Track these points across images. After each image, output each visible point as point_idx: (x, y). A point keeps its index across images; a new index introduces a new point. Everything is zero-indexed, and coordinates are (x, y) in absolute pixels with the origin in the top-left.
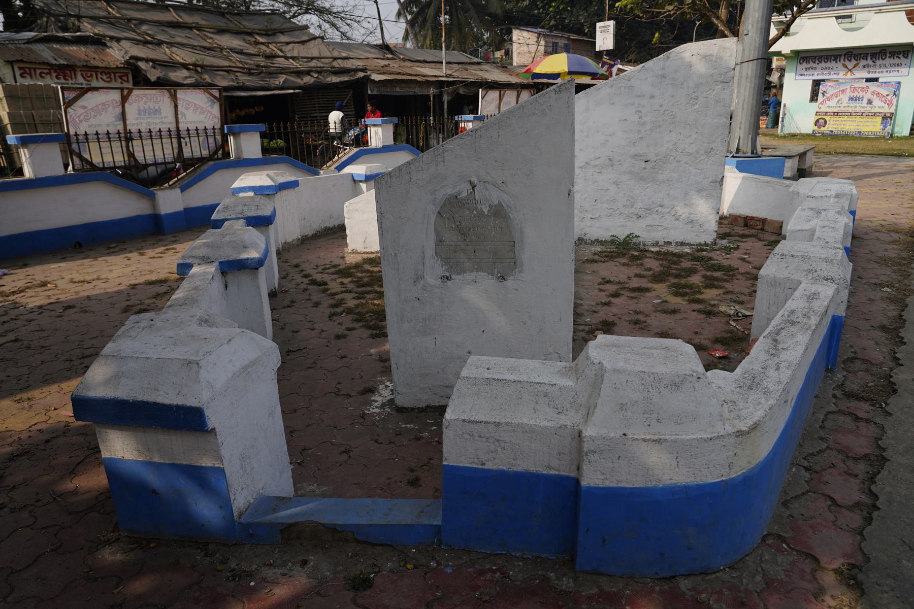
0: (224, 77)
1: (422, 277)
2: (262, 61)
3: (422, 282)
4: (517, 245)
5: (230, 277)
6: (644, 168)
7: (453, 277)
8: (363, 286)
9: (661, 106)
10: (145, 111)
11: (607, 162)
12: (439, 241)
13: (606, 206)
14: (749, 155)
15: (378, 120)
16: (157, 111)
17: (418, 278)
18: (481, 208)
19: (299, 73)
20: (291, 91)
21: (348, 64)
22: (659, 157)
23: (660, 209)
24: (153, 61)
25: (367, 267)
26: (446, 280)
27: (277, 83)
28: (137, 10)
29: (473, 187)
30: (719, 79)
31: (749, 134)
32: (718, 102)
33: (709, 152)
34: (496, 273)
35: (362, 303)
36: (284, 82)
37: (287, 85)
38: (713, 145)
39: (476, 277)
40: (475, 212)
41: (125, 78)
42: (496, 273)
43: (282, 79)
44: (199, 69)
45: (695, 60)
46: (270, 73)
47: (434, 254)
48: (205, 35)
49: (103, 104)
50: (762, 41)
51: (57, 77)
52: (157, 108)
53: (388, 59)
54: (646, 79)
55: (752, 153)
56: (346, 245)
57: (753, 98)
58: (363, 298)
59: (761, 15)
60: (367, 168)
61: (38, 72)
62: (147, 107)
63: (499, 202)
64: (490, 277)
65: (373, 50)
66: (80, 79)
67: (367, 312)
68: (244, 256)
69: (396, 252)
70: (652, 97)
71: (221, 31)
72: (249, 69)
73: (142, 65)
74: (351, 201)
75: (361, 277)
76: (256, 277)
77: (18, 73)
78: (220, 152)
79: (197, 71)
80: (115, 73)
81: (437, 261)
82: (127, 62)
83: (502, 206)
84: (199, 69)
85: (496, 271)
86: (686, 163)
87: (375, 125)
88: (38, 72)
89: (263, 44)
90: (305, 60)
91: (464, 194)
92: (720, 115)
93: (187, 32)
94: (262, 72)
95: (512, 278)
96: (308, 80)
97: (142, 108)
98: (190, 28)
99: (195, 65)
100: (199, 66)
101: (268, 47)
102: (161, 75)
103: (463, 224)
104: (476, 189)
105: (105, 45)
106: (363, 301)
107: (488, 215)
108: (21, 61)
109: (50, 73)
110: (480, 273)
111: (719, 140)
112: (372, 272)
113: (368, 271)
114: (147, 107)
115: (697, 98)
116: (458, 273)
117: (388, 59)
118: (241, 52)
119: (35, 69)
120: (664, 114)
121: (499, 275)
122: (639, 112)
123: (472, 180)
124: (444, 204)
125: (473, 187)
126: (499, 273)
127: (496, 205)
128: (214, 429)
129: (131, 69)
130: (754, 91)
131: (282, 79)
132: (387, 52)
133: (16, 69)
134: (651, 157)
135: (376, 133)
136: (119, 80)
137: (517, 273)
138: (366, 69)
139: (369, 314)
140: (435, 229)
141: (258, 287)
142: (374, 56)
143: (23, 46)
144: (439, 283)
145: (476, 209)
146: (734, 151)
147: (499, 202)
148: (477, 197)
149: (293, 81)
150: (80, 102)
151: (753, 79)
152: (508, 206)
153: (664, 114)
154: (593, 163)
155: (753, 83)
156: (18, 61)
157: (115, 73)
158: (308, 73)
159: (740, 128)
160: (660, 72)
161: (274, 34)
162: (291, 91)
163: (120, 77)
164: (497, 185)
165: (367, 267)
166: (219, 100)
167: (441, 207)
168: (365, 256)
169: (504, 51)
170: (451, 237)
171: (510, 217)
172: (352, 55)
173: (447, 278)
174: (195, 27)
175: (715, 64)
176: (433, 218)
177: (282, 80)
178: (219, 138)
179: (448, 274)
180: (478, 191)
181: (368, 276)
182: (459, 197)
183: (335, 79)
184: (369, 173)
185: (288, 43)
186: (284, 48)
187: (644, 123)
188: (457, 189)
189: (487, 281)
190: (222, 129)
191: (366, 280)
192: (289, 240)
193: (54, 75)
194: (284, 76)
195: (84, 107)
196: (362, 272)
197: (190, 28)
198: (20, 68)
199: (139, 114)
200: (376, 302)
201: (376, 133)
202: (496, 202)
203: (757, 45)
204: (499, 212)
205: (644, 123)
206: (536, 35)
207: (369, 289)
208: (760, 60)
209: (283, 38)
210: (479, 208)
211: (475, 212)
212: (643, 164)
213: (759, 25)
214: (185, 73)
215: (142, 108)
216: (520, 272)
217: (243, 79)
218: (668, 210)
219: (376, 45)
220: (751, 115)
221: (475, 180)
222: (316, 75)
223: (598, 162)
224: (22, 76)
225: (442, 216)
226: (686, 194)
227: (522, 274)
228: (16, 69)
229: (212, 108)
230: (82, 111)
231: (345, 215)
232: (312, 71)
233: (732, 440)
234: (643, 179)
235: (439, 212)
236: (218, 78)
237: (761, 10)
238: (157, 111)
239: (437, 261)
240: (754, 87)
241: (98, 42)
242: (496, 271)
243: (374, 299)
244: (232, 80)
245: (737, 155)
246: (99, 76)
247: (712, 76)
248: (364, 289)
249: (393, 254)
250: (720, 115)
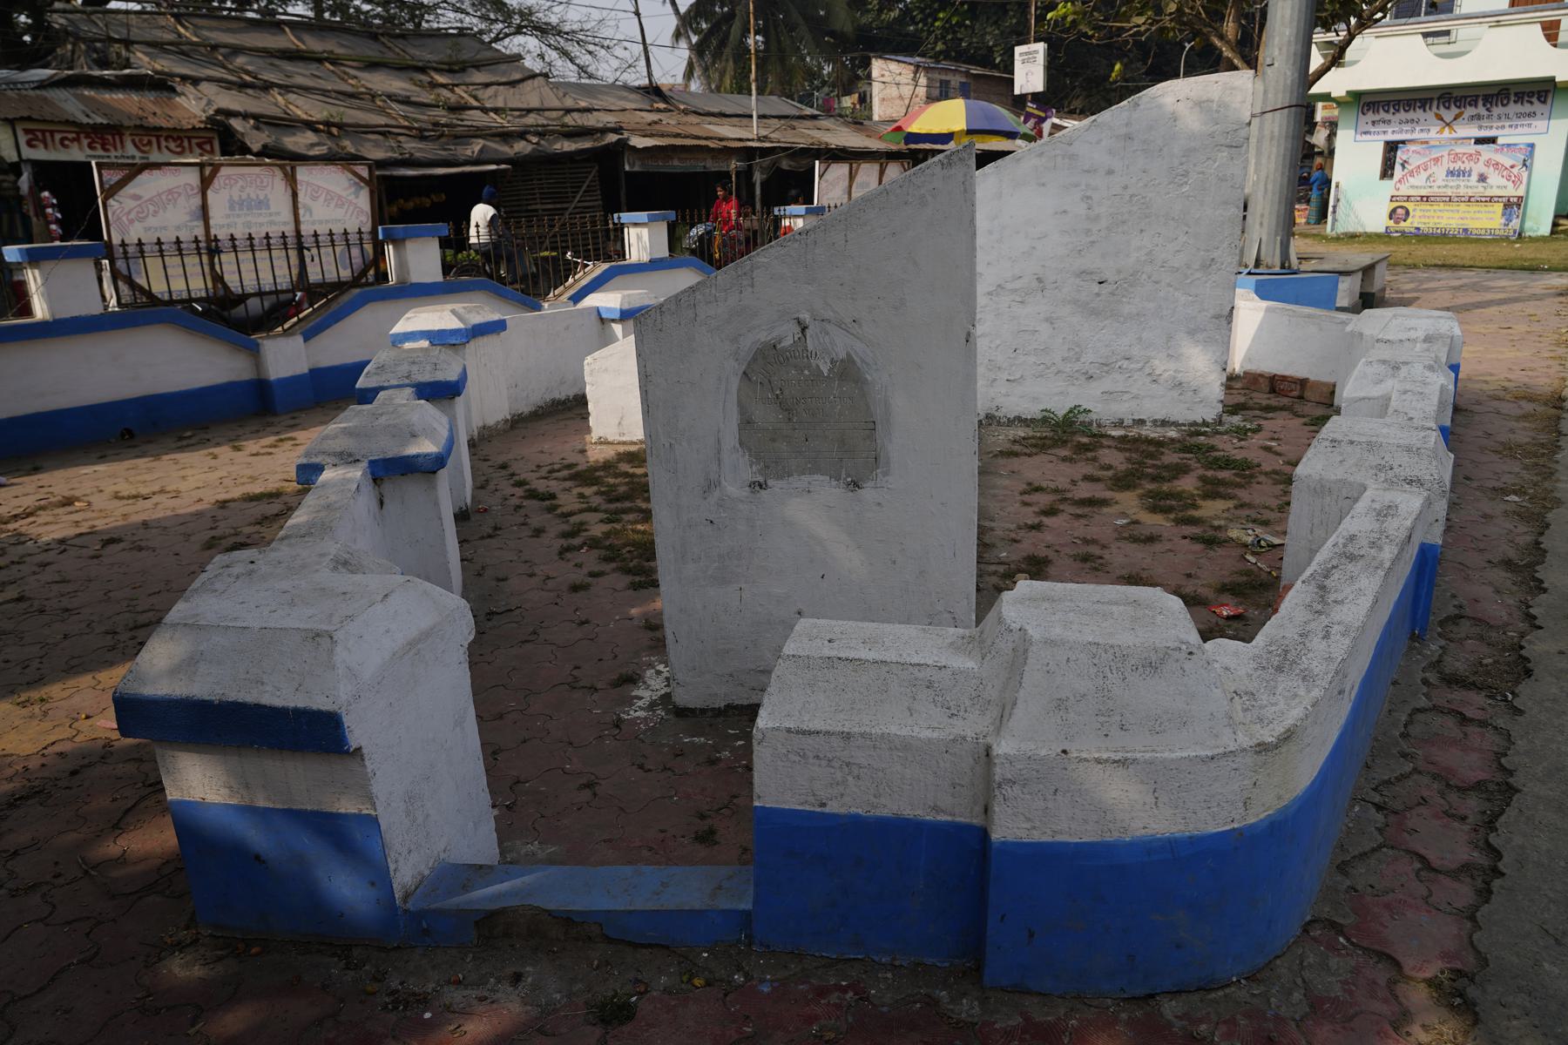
0: (377, 144)
1: (718, 484)
2: (443, 116)
3: (717, 493)
4: (879, 427)
5: (387, 487)
6: (1098, 295)
7: (770, 483)
8: (618, 500)
9: (1126, 187)
10: (241, 203)
11: (1035, 284)
12: (746, 422)
13: (1032, 359)
14: (1277, 269)
15: (642, 216)
16: (262, 204)
17: (711, 485)
18: (818, 366)
19: (506, 136)
20: (493, 167)
21: (591, 120)
22: (1122, 277)
23: (1125, 364)
24: (256, 117)
25: (625, 467)
26: (757, 488)
27: (469, 152)
28: (229, 30)
29: (804, 329)
30: (1223, 142)
31: (1276, 235)
32: (1222, 179)
33: (1208, 265)
34: (843, 476)
35: (615, 529)
36: (481, 151)
37: (485, 156)
38: (1215, 254)
39: (809, 483)
40: (806, 372)
41: (208, 147)
42: (843, 476)
43: (477, 146)
44: (335, 130)
45: (1182, 109)
46: (456, 137)
47: (738, 445)
48: (345, 73)
49: (170, 192)
50: (1296, 75)
51: (90, 146)
52: (262, 198)
53: (659, 110)
54: (1098, 142)
55: (1283, 267)
56: (588, 430)
57: (1283, 173)
58: (618, 521)
59: (1295, 31)
60: (624, 298)
61: (58, 137)
62: (244, 196)
63: (848, 355)
64: (834, 483)
65: (633, 96)
66: (131, 150)
67: (625, 545)
68: (412, 450)
69: (673, 442)
70: (1110, 172)
71: (372, 66)
72: (421, 130)
73: (236, 124)
74: (596, 354)
75: (614, 485)
76: (433, 487)
77: (22, 139)
78: (372, 272)
79: (331, 134)
80: (189, 139)
81: (743, 456)
82: (210, 119)
83: (854, 362)
84: (335, 130)
85: (844, 472)
86: (1169, 285)
87: (636, 225)
88: (58, 137)
89: (444, 86)
90: (517, 113)
91: (788, 342)
92: (1226, 203)
93: (313, 68)
94: (442, 135)
95: (870, 484)
96: (522, 147)
97: (236, 198)
98: (318, 60)
99: (328, 124)
100: (334, 125)
101: (452, 91)
102: (268, 140)
103: (786, 392)
104: (808, 333)
105: (173, 90)
106: (618, 526)
107: (828, 377)
108: (29, 119)
109: (77, 140)
110: (816, 477)
111: (1225, 245)
112: (633, 475)
113: (626, 475)
114: (244, 196)
115: (1186, 174)
116: (779, 477)
117: (659, 110)
118: (406, 101)
119: (52, 133)
120: (1130, 201)
121: (849, 479)
122: (1089, 198)
123: (801, 316)
124: (754, 359)
125: (804, 329)
126: (848, 476)
127: (842, 361)
128: (359, 749)
129: (220, 134)
130: (1284, 159)
131: (477, 146)
132: (657, 99)
133: (20, 134)
134: (1109, 275)
135: (639, 238)
136: (198, 151)
137: (880, 475)
138: (621, 128)
139: (628, 549)
140: (740, 404)
141: (436, 504)
142: (634, 106)
143: (31, 93)
144: (744, 494)
145: (809, 367)
146: (1252, 263)
147: (848, 355)
148: (810, 347)
149: (496, 150)
150: (130, 189)
151: (1282, 141)
152: (863, 361)
153: (1130, 201)
154: (1009, 286)
155: (1283, 147)
156: (22, 119)
157: (189, 139)
158: (522, 135)
159: (1261, 224)
160: (1124, 131)
161: (463, 70)
162: (493, 167)
163: (200, 145)
164: (843, 326)
165: (625, 467)
166: (368, 182)
167: (749, 364)
168: (622, 449)
169: (857, 95)
170: (766, 415)
171: (866, 379)
172: (596, 104)
173: (760, 486)
174: (327, 59)
175: (1216, 115)
176: (735, 382)
177: (477, 148)
178: (369, 248)
179: (761, 479)
180: (811, 336)
181: (627, 484)
182: (778, 347)
183: (568, 146)
184: (626, 307)
185: (487, 85)
186: (480, 94)
187: (1097, 218)
188: (775, 334)
189: (828, 491)
190: (374, 232)
191: (622, 489)
192: (491, 422)
193: (85, 142)
194: (481, 142)
195: (136, 197)
196: (616, 476)
197: (320, 61)
198: (27, 131)
199: (232, 208)
200: (639, 527)
201: (639, 238)
202: (842, 355)
203: (1289, 82)
204: (847, 371)
205: (1097, 218)
206: (912, 68)
207: (627, 504)
208: (1286, 110)
209: (479, 77)
210: (814, 365)
211: (806, 372)
212: (1096, 288)
213: (1292, 49)
214: (310, 137)
215: (236, 198)
216: (886, 474)
217: (411, 146)
218: (1139, 366)
219: (639, 88)
220: (1280, 202)
221: (806, 317)
222: (535, 140)
223: (1018, 284)
224: (30, 144)
225: (750, 380)
226: (1170, 338)
227: (887, 478)
228: (20, 134)
229: (357, 197)
230: (132, 204)
231: (587, 379)
232: (529, 132)
233: (1249, 759)
234: (1095, 313)
235: (744, 373)
236: (368, 145)
237: (1295, 24)
238: (262, 204)
239: (743, 456)
240: (1284, 155)
241: (160, 85)
242: (844, 472)
243: (636, 522)
244: (392, 149)
245: (1257, 271)
246: (164, 143)
247: (1212, 135)
248: (618, 505)
249: (667, 445)
250: (1226, 203)
